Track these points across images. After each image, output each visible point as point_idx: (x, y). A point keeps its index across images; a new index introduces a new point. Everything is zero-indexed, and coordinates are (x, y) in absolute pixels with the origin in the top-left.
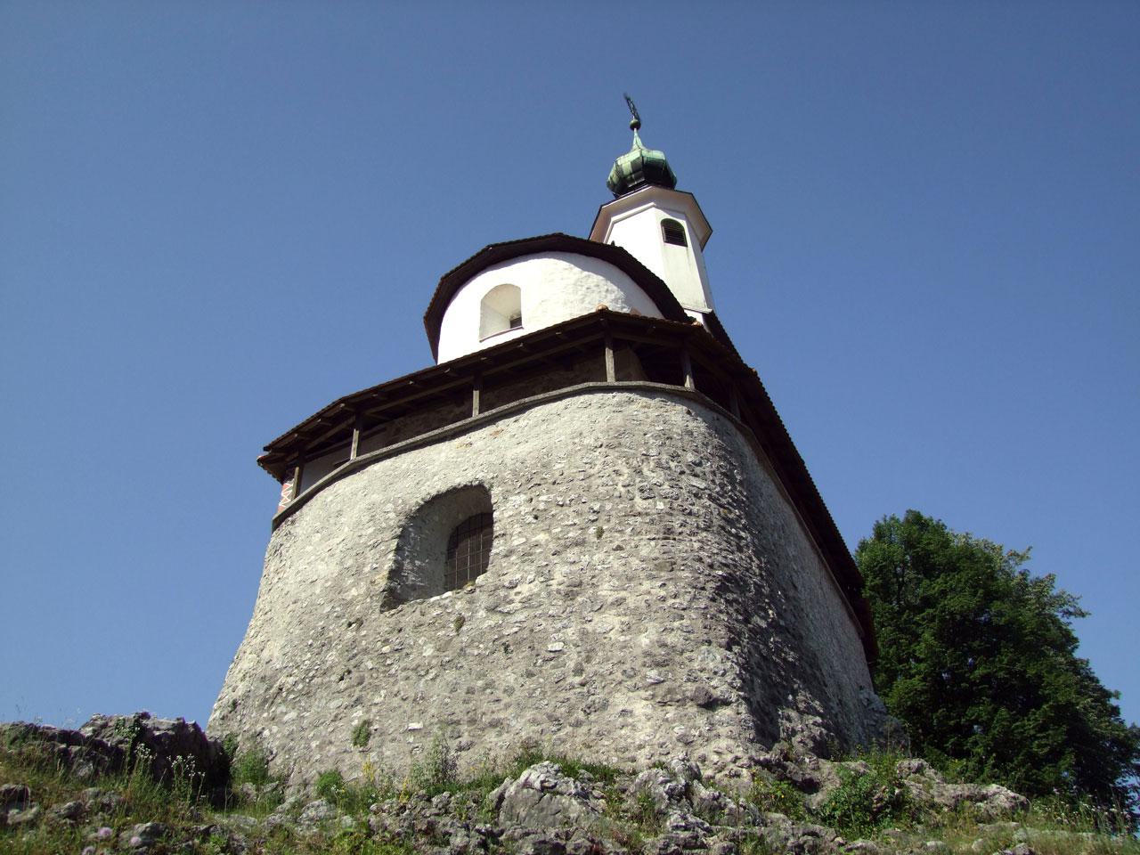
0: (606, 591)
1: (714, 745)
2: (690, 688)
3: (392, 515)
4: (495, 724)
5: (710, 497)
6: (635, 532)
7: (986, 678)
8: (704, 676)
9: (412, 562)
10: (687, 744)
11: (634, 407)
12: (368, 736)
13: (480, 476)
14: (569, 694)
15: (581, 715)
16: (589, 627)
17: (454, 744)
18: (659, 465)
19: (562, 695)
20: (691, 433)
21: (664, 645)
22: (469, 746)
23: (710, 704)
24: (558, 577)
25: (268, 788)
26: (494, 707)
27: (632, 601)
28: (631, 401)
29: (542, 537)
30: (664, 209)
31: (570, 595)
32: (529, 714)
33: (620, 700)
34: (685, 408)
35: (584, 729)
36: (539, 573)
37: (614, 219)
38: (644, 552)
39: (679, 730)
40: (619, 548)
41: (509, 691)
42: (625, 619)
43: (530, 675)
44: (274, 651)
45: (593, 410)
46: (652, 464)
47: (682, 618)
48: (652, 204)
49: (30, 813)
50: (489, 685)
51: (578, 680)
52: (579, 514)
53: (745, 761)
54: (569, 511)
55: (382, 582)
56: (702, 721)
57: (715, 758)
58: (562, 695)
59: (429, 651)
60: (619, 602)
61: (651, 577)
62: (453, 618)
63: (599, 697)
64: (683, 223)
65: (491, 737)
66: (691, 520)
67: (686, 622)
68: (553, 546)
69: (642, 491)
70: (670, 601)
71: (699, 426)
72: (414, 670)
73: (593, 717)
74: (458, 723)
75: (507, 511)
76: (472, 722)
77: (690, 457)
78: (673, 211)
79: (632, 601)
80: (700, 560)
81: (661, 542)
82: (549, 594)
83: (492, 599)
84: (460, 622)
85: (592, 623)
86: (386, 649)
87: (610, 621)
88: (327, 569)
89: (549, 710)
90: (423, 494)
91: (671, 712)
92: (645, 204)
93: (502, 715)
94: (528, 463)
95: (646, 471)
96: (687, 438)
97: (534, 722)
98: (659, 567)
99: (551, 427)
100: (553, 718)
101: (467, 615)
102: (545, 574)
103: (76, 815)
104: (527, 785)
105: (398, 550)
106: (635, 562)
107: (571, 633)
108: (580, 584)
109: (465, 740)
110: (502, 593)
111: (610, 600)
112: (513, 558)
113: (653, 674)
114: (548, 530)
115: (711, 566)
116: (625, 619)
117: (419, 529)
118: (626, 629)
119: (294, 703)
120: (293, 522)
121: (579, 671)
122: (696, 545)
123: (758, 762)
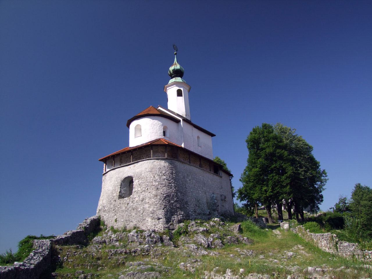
0: (147, 201)
1: (159, 225)
2: (156, 217)
3: (119, 180)
4: (132, 221)
5: (167, 180)
6: (152, 189)
7: (275, 167)
8: (159, 215)
9: (123, 189)
10: (155, 225)
11: (155, 162)
12: (117, 221)
13: (132, 175)
14: (141, 218)
15: (142, 221)
16: (144, 207)
17: (127, 224)
18: (158, 175)
19: (140, 218)
20: (165, 167)
21: (153, 210)
22: (128, 224)
23: (159, 219)
24: (141, 197)
25: (105, 227)
26: (132, 219)
27: (150, 202)
28: (155, 161)
29: (139, 189)
30: (178, 86)
31: (142, 201)
32: (136, 220)
33: (147, 219)
34: (164, 161)
35: (142, 223)
36: (138, 196)
37: (168, 88)
38: (153, 193)
39: (154, 223)
40: (150, 192)
41: (134, 216)
42: (149, 205)
43: (136, 214)
44: (104, 201)
45: (148, 164)
46: (157, 175)
47: (157, 205)
48: (175, 85)
49: (76, 253)
50: (131, 215)
51: (142, 215)
52: (145, 185)
53: (163, 227)
54: (144, 184)
55: (118, 194)
56: (157, 222)
57: (158, 227)
58: (140, 218)
59: (124, 208)
60: (148, 202)
61: (153, 198)
62: (127, 203)
63: (144, 218)
64: (182, 89)
65: (131, 223)
66: (162, 186)
67: (157, 206)
68: (141, 191)
69: (154, 181)
70: (155, 202)
71: (167, 164)
72: (122, 211)
73: (143, 221)
74: (127, 221)
75: (136, 183)
76: (129, 221)
77: (164, 172)
78: (180, 86)
79: (150, 202)
80: (162, 194)
81: (156, 191)
82: (139, 200)
83: (132, 200)
84: (128, 204)
85: (129, 225)
86: (119, 207)
87: (147, 206)
88: (111, 188)
89: (138, 220)
90: (124, 177)
91: (153, 220)
92: (173, 85)
93: (132, 220)
94: (139, 173)
95: (156, 177)
96: (164, 168)
97: (136, 222)
98: (155, 196)
99: (143, 166)
100: (138, 221)
101: (129, 202)
102: (139, 196)
103: (80, 253)
104: (131, 235)
105: (121, 187)
106: (152, 195)
107: (142, 208)
108: (143, 199)
109: (128, 223)
110: (134, 199)
111: (147, 202)
112: (135, 193)
113: (151, 215)
114: (140, 188)
115: (164, 194)
116: (149, 205)
117: (124, 183)
118: (149, 207)
119: (108, 213)
120: (106, 176)
121: (142, 214)
122: (162, 190)
123: (165, 227)
